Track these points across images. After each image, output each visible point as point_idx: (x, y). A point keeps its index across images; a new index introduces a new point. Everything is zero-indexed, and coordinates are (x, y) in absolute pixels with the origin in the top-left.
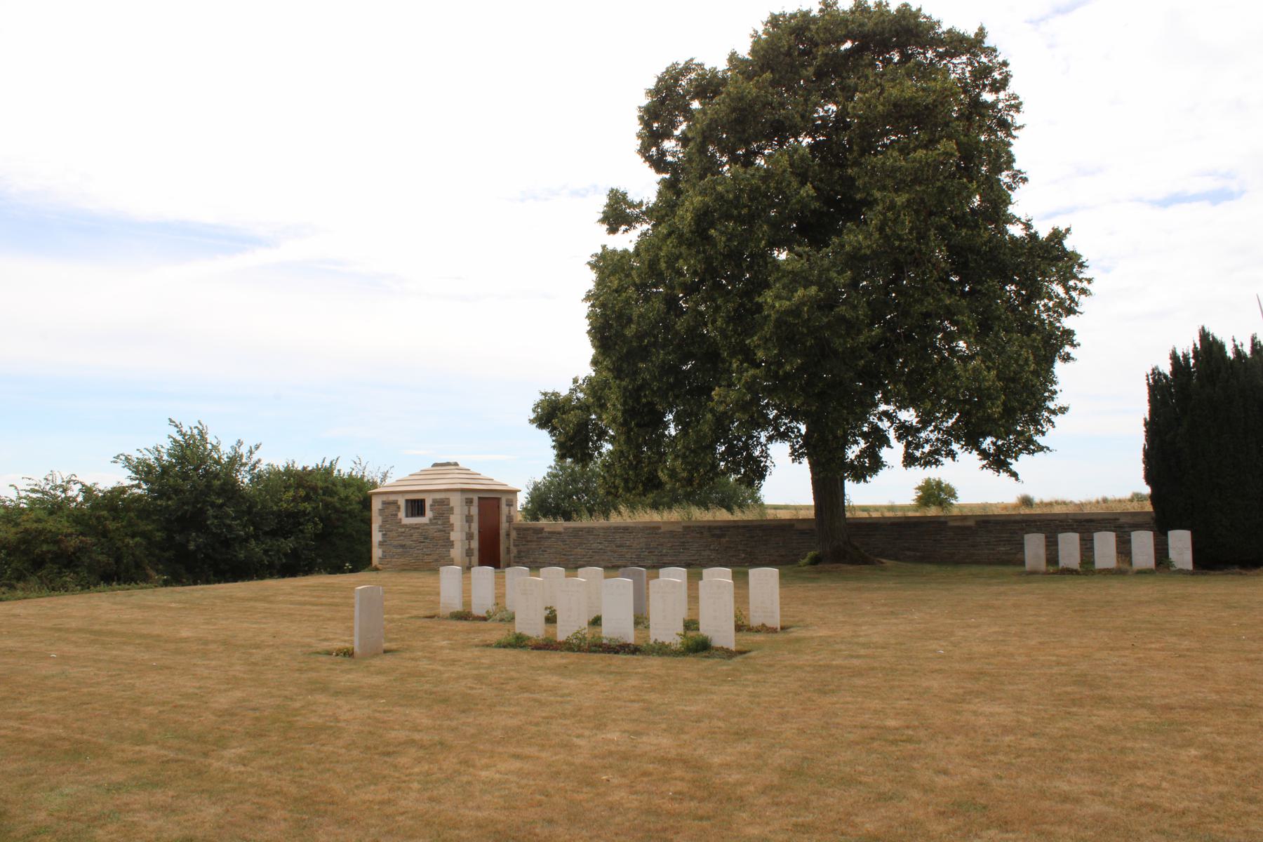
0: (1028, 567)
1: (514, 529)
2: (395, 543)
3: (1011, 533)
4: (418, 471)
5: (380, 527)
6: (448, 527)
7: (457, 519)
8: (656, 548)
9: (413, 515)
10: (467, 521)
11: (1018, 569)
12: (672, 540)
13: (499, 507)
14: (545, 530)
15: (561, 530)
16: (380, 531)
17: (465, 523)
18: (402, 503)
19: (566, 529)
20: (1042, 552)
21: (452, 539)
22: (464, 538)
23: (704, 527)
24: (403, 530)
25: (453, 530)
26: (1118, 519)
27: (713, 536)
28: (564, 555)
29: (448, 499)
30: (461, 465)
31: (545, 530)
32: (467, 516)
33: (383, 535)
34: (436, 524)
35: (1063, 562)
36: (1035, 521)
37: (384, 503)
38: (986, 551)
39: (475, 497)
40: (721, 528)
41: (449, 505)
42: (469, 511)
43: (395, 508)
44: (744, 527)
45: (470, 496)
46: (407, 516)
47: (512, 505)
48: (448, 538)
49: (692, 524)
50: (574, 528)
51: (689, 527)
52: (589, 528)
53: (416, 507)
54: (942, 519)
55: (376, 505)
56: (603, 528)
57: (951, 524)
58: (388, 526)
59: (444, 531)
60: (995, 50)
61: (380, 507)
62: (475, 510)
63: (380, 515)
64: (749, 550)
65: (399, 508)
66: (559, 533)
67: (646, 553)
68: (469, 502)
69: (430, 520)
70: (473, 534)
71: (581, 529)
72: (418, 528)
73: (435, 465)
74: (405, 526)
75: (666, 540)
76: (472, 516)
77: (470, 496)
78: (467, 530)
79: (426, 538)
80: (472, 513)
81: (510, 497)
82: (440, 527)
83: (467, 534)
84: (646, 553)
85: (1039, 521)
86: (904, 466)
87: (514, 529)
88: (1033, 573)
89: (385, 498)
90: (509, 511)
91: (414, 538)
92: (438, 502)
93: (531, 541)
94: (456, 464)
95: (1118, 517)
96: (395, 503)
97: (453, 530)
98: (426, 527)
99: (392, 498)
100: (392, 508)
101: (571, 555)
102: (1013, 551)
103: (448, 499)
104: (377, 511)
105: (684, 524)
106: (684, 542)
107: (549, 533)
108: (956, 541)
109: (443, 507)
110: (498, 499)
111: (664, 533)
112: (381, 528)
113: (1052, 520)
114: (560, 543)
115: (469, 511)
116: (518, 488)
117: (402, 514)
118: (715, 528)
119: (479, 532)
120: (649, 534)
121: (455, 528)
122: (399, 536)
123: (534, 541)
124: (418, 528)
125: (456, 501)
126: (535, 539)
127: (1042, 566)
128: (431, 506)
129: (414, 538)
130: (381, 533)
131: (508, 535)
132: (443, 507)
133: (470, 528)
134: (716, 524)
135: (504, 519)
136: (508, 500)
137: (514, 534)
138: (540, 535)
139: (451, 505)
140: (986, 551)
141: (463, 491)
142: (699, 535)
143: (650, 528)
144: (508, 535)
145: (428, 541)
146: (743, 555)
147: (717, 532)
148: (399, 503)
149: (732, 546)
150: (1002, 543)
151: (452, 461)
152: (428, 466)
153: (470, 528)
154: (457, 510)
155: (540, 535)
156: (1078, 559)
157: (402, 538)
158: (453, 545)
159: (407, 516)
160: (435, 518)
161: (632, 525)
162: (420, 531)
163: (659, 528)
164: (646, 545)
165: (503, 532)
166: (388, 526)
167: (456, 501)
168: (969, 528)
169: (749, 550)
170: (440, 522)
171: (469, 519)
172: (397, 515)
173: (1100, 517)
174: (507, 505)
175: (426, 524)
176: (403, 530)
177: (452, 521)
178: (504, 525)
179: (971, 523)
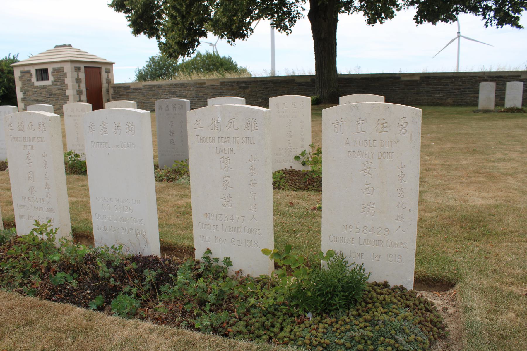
0: (480, 107)
1: (112, 87)
2: (32, 99)
3: (444, 85)
4: (45, 51)
5: (21, 88)
6: (63, 87)
7: (69, 81)
8: (203, 97)
9: (42, 80)
10: (77, 82)
11: (474, 109)
12: (213, 91)
13: (100, 73)
14: (131, 87)
15: (141, 87)
16: (21, 91)
17: (75, 83)
18: (33, 72)
19: (144, 86)
20: (493, 95)
21: (67, 94)
22: (76, 93)
23: (234, 82)
24: (36, 90)
25: (67, 88)
26: (520, 76)
27: (240, 88)
28: (144, 103)
29: (63, 67)
30: (74, 46)
31: (131, 87)
32: (76, 79)
33: (24, 93)
34: (56, 85)
35: (508, 104)
36: (461, 77)
37: (22, 72)
38: (426, 97)
39: (82, 66)
40: (245, 82)
41: (63, 71)
42: (78, 75)
43: (30, 76)
44: (261, 81)
45: (78, 65)
46: (37, 80)
47: (109, 72)
48: (65, 94)
49: (226, 80)
50: (149, 85)
51: (224, 82)
52: (159, 85)
53: (42, 74)
54: (397, 76)
55: (17, 74)
56: (168, 85)
57: (403, 79)
58: (26, 88)
59: (62, 89)
60: (241, 270)
61: (20, 76)
62: (82, 75)
63: (20, 81)
64: (264, 96)
65: (31, 75)
66: (140, 89)
67: (196, 100)
68: (78, 69)
69: (52, 82)
70: (82, 91)
71: (154, 86)
72: (45, 88)
73: (57, 47)
74: (37, 87)
75: (210, 91)
76: (81, 79)
77: (78, 65)
78: (78, 88)
79: (51, 95)
80: (80, 77)
81: (108, 67)
82: (59, 87)
83: (77, 91)
84: (196, 100)
85: (465, 77)
86: (393, 17)
87: (112, 87)
88: (486, 111)
89: (22, 69)
90: (108, 76)
91: (43, 95)
92: (56, 70)
93: (122, 95)
94: (70, 46)
95: (520, 74)
96: (29, 72)
97: (67, 88)
98: (50, 87)
99: (26, 69)
100: (28, 75)
101: (148, 103)
102: (445, 97)
103: (63, 67)
104: (18, 78)
105: (221, 81)
106: (221, 92)
107: (134, 89)
108: (406, 90)
109: (59, 73)
110: (100, 68)
111: (208, 87)
112: (22, 90)
113: (473, 77)
114: (140, 95)
115: (78, 75)
116: (114, 62)
117: (34, 79)
118: (242, 82)
119: (87, 89)
120: (198, 87)
121: (69, 87)
122: (34, 94)
123: (124, 95)
124: (45, 88)
125: (68, 68)
126: (125, 93)
127: (492, 107)
128: (52, 73)
129: (43, 95)
130: (22, 93)
131: (108, 91)
132: (59, 73)
133: (79, 86)
134: (242, 80)
135: (104, 81)
136: (106, 69)
137: (111, 91)
138: (128, 91)
139: (65, 71)
140: (426, 97)
141: (72, 61)
142: (231, 88)
143: (199, 84)
144: (108, 91)
145: (52, 96)
146: (261, 100)
147: (243, 85)
148: (31, 72)
149: (253, 94)
150: (438, 92)
151: (67, 44)
152: (52, 47)
153: (79, 86)
154: (69, 75)
155: (128, 91)
156: (493, 104)
157: (36, 95)
158: (68, 98)
159: (37, 80)
160: (55, 81)
161: (187, 82)
162: (46, 90)
163: (204, 83)
164: (196, 95)
165: (104, 90)
166: (26, 88)
167: (68, 68)
168: (415, 81)
169: (264, 96)
170: (59, 84)
171: (78, 81)
172: (30, 80)
173: (507, 75)
174: (106, 72)
175: (50, 85)
176: (36, 90)
177: (66, 83)
178: (105, 86)
179: (417, 78)
